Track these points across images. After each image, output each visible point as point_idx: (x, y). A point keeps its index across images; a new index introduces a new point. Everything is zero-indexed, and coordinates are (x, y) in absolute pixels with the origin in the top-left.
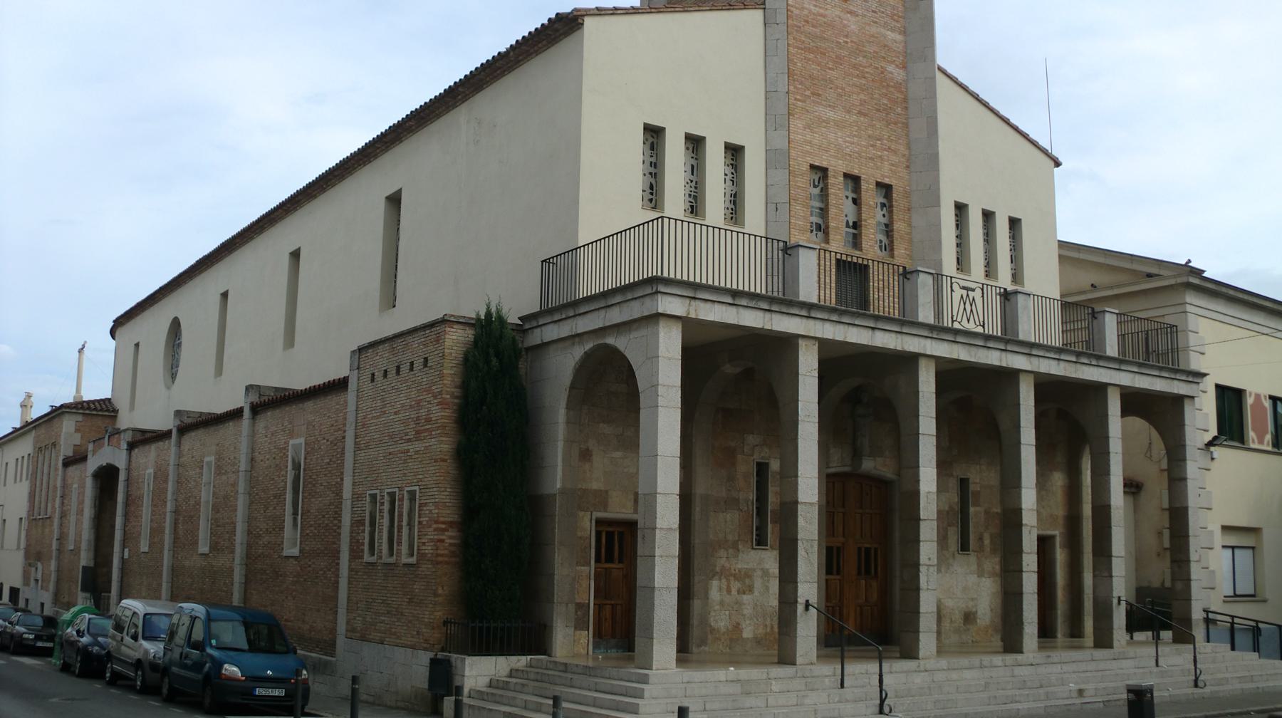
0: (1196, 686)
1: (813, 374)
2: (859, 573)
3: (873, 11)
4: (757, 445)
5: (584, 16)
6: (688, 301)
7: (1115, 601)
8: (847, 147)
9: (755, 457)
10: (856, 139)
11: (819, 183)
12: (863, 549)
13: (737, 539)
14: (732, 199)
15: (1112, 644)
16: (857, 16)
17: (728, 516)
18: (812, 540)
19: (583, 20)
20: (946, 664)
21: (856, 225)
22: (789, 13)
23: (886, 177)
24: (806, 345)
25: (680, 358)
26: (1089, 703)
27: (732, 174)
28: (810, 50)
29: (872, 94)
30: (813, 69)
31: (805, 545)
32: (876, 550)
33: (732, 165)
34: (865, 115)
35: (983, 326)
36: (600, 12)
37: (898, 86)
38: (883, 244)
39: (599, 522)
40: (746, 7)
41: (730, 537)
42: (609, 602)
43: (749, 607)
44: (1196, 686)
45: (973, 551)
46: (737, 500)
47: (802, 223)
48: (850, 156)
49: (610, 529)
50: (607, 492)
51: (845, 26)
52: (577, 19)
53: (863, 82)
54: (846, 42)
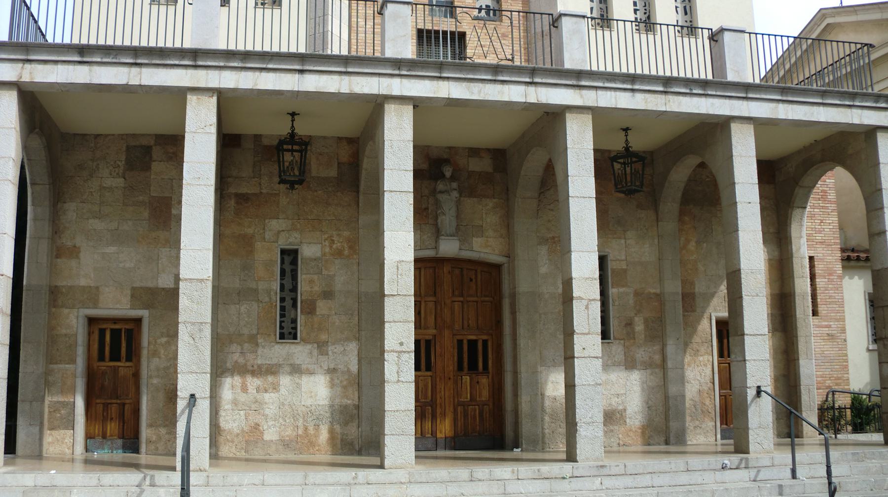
2: (460, 368)
4: (283, 231)
6: (20, 65)
7: (751, 393)
12: (465, 342)
13: (255, 332)
17: (242, 308)
18: (201, 323)
31: (189, 329)
32: (485, 342)
41: (246, 331)
45: (615, 339)
46: (256, 291)
50: (97, 288)
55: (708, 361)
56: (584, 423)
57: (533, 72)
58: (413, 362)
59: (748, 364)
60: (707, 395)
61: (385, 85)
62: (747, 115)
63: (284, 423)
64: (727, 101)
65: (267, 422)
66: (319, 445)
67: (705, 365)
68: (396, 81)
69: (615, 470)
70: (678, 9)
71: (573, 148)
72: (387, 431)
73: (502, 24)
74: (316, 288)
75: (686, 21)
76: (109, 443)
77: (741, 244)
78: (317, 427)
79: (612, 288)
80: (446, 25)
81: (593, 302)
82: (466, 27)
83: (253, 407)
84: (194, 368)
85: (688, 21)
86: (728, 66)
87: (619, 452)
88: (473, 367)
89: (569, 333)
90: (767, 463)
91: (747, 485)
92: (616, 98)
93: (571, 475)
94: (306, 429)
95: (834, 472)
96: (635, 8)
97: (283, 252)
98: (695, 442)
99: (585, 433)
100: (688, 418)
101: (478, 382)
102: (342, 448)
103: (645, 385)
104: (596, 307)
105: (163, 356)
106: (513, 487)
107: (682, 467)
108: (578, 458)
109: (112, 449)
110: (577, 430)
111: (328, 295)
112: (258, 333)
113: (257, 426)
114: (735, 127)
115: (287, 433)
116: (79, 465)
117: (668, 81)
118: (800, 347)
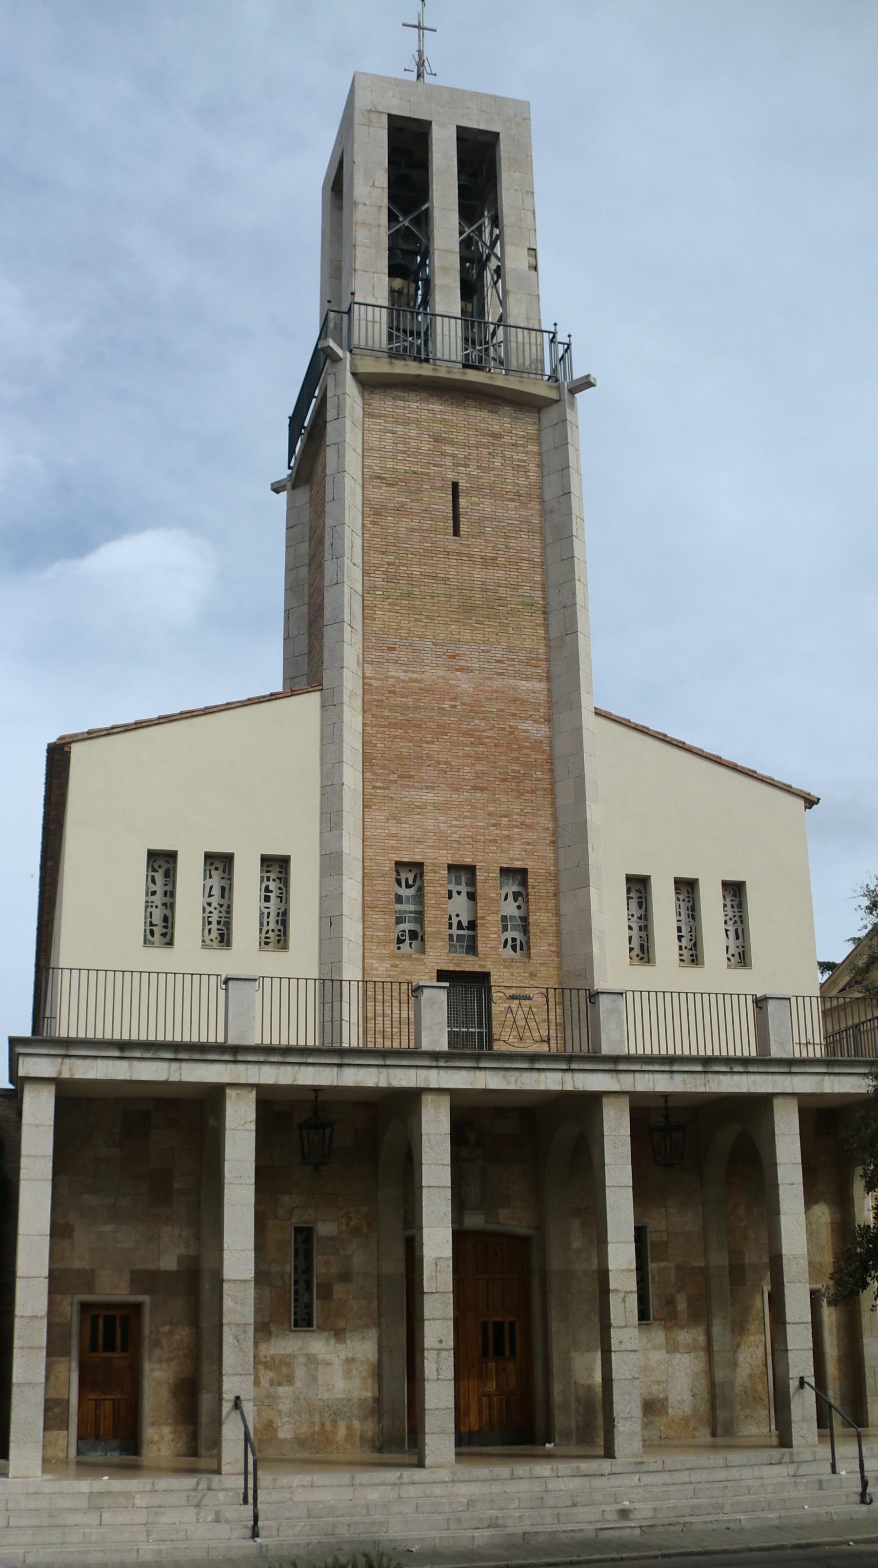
0: (863, 1501)
1: (248, 1128)
2: (485, 1353)
3: (497, 661)
4: (296, 1207)
5: (70, 743)
6: (59, 1060)
7: (794, 1384)
8: (454, 832)
9: (293, 1221)
10: (467, 822)
11: (414, 881)
12: (490, 1325)
13: (267, 1319)
14: (280, 918)
15: (791, 1442)
16: (472, 671)
18: (245, 1324)
19: (70, 748)
20: (450, 1475)
21: (472, 925)
22: (366, 687)
23: (518, 860)
24: (237, 1094)
25: (52, 1123)
26: (611, 1529)
27: (280, 889)
28: (396, 726)
29: (495, 762)
30: (402, 747)
31: (233, 1331)
32: (512, 1325)
33: (279, 879)
34: (482, 789)
35: (548, 1041)
36: (92, 735)
37: (537, 745)
38: (518, 943)
39: (85, 1307)
40: (294, 693)
42: (108, 1397)
43: (286, 1402)
44: (863, 1501)
45: (655, 1319)
47: (383, 934)
48: (459, 842)
49: (111, 1313)
50: (93, 1271)
51: (452, 687)
52: (63, 748)
53: (481, 749)
54: (454, 706)
55: (760, 1340)
56: (622, 1418)
57: (570, 1059)
58: (452, 1359)
59: (790, 1355)
60: (758, 1380)
61: (423, 1077)
62: (790, 1091)
63: (299, 1419)
64: (770, 1077)
65: (281, 1418)
66: (337, 1443)
67: (757, 1346)
68: (434, 1073)
69: (652, 1467)
70: (728, 933)
71: (610, 1135)
72: (427, 1430)
73: (531, 961)
74: (333, 1270)
75: (738, 947)
76: (103, 1444)
77: (782, 1228)
78: (334, 1423)
79: (652, 1261)
80: (469, 964)
81: (630, 1294)
82: (491, 967)
83: (266, 1402)
84: (239, 1369)
85: (740, 947)
86: (771, 1037)
87: (661, 1446)
88: (499, 1351)
89: (605, 1326)
90: (809, 1457)
91: (783, 1480)
92: (654, 1081)
93: (609, 1472)
94: (323, 1425)
95: (867, 1467)
96: (680, 934)
97: (297, 1230)
98: (746, 1433)
99: (622, 1429)
100: (738, 1407)
101: (504, 1369)
102: (361, 1446)
103: (688, 1371)
104: (633, 1300)
105: (166, 1347)
106: (553, 1485)
107: (721, 1462)
108: (616, 1454)
109: (106, 1451)
110: (614, 1426)
111: (345, 1277)
112: (271, 1321)
113: (271, 1422)
114: (777, 1103)
115: (303, 1431)
116: (72, 1467)
117: (707, 1061)
118: (863, 1323)
